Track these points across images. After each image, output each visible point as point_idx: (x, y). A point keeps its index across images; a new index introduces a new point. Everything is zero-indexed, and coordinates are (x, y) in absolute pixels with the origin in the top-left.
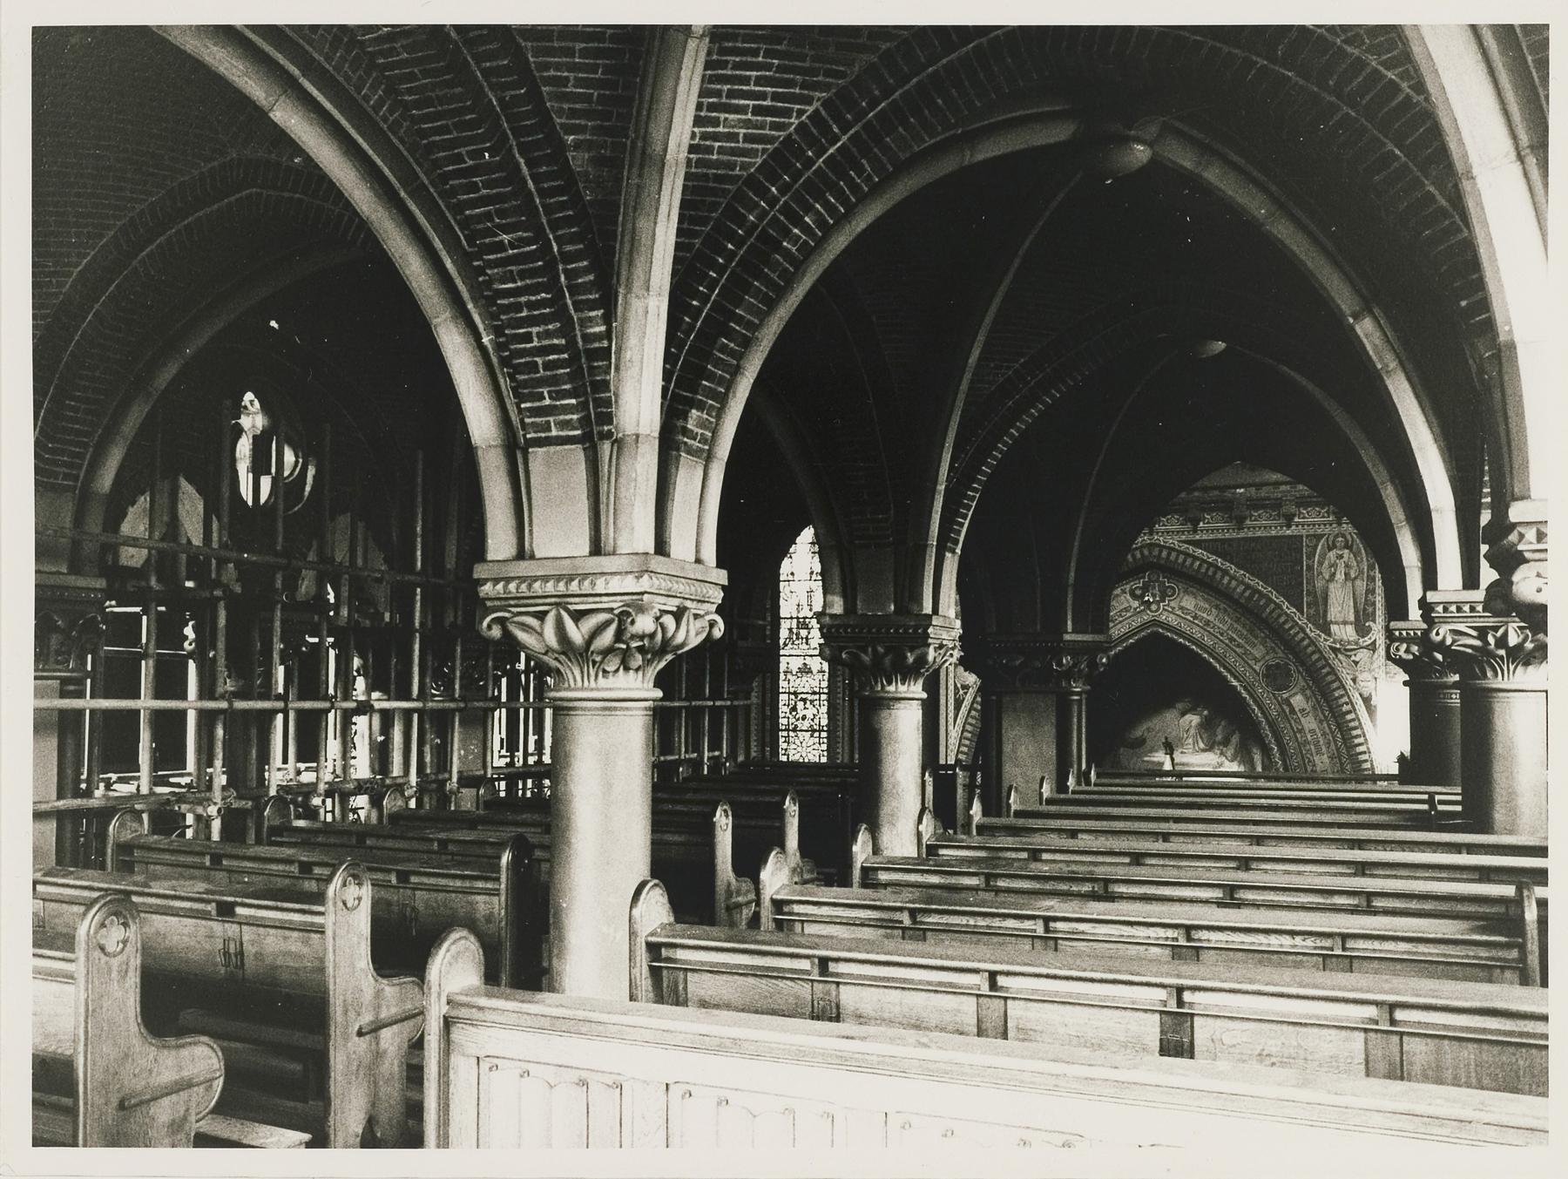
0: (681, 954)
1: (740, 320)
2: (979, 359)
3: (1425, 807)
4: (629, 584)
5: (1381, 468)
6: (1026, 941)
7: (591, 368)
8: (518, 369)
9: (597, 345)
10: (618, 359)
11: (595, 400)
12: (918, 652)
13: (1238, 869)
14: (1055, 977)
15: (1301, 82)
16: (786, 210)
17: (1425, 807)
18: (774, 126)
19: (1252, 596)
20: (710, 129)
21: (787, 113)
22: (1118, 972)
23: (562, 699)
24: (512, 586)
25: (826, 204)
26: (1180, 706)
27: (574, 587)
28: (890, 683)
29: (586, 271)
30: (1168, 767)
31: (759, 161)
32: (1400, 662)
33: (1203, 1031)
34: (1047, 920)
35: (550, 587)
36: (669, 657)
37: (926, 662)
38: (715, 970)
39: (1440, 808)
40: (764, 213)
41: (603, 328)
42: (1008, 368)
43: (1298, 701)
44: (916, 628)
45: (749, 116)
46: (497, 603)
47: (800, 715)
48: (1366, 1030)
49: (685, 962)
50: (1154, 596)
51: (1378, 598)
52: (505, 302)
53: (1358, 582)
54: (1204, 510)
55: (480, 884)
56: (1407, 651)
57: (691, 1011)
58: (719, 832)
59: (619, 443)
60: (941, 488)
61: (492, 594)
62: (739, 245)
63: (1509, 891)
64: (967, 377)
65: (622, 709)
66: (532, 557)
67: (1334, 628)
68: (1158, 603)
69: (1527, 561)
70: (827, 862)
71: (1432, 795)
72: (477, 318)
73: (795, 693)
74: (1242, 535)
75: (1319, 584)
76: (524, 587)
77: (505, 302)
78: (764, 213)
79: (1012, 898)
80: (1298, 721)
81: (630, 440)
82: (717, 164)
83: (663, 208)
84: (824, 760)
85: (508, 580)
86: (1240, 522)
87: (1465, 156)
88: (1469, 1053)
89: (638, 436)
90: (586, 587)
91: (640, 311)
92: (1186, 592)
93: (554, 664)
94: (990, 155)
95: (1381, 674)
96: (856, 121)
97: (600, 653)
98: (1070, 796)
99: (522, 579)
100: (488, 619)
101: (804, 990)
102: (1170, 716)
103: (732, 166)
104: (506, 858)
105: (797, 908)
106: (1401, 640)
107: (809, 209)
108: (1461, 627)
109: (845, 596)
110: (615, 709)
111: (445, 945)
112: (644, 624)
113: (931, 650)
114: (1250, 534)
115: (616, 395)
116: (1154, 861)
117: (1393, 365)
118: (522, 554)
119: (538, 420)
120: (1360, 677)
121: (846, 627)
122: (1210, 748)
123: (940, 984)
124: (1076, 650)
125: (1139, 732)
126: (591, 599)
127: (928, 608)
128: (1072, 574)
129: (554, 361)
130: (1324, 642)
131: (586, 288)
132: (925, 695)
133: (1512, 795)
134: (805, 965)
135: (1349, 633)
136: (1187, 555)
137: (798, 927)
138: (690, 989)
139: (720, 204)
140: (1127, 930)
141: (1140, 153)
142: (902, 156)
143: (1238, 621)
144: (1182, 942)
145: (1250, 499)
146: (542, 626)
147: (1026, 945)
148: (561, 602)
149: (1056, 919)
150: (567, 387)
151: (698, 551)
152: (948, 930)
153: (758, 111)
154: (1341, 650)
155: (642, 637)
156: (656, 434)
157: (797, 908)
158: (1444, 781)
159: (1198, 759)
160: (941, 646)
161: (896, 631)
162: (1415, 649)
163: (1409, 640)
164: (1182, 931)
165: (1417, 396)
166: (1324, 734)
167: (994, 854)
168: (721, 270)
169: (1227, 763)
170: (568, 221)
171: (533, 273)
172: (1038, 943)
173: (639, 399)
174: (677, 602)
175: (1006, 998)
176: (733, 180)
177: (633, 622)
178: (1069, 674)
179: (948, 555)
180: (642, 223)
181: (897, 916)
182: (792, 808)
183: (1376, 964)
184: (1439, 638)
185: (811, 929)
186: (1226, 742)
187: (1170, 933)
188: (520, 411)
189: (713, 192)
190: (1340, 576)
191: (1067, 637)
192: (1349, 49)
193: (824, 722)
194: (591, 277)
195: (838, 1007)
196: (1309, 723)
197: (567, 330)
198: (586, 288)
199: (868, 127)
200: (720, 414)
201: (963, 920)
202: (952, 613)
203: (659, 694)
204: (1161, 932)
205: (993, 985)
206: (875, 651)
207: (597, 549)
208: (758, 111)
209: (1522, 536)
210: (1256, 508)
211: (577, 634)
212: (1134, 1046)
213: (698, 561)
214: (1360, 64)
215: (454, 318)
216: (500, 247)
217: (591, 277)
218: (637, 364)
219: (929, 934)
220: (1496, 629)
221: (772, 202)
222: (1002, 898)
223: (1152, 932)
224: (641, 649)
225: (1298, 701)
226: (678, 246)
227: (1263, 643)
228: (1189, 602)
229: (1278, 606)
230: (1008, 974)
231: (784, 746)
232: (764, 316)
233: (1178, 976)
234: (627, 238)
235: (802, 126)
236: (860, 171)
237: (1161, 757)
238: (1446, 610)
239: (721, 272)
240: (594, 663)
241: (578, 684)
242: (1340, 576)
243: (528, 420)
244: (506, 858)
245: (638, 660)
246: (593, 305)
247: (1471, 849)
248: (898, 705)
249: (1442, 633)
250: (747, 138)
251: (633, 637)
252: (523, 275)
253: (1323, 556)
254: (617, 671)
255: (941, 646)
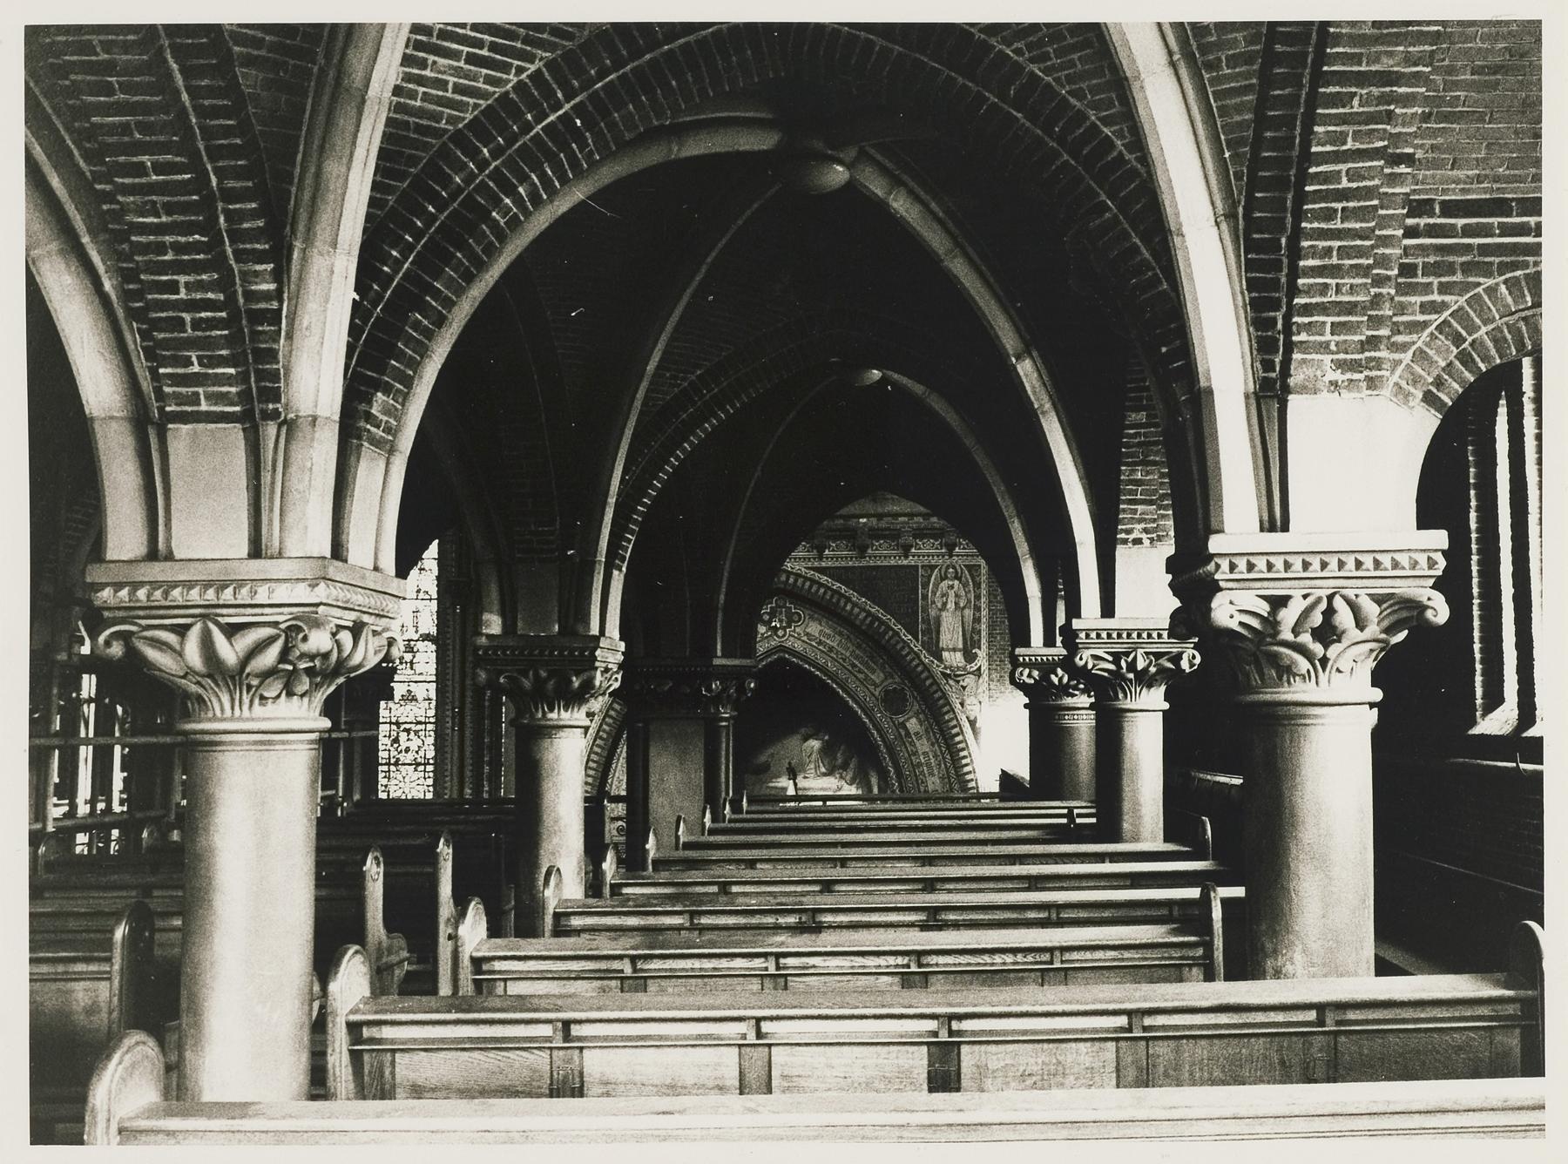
0: (387, 1032)
1: (437, 294)
2: (658, 368)
3: (1064, 821)
4: (302, 594)
5: (1009, 502)
6: (755, 980)
7: (255, 335)
8: (157, 325)
9: (263, 305)
10: (291, 324)
11: (257, 372)
12: (585, 676)
13: (821, 892)
14: (827, 1017)
15: (1028, 124)
16: (497, 175)
17: (1064, 821)
18: (489, 80)
19: (872, 623)
20: (416, 71)
21: (505, 68)
22: (891, 1006)
23: (195, 732)
24: (142, 594)
25: (543, 177)
26: (803, 730)
27: (227, 596)
28: (552, 710)
29: (254, 215)
30: (791, 792)
31: (469, 117)
32: (1022, 687)
33: (969, 1057)
34: (778, 956)
35: (194, 595)
36: (341, 680)
37: (593, 687)
38: (430, 1047)
39: (1078, 821)
40: (472, 176)
41: (272, 287)
42: (684, 379)
43: (913, 724)
44: (582, 651)
45: (462, 64)
46: (121, 614)
47: (403, 747)
48: (1117, 1040)
49: (393, 1041)
50: (781, 621)
51: (983, 627)
52: (142, 239)
53: (967, 612)
54: (829, 538)
55: (80, 967)
56: (1030, 676)
57: (401, 1103)
58: (369, 885)
59: (290, 427)
60: (612, 500)
61: (112, 602)
62: (440, 210)
63: (1194, 893)
64: (644, 385)
65: (283, 742)
66: (169, 557)
67: (945, 654)
68: (784, 629)
69: (1221, 589)
70: (516, 912)
71: (1071, 809)
72: (96, 259)
73: (398, 724)
74: (864, 563)
75: (933, 613)
76: (158, 594)
77: (142, 239)
78: (472, 176)
79: (739, 936)
80: (912, 744)
81: (304, 424)
82: (420, 113)
83: (360, 153)
84: (430, 796)
85: (135, 586)
86: (862, 551)
87: (1177, 215)
88: (1201, 1050)
89: (315, 419)
90: (244, 596)
91: (324, 274)
92: (811, 617)
93: (194, 688)
94: (696, 152)
95: (984, 698)
96: (583, 89)
97: (257, 676)
98: (726, 824)
99: (155, 585)
100: (108, 632)
101: (540, 1060)
102: (793, 742)
103: (437, 117)
104: (120, 933)
105: (498, 965)
106: (1025, 665)
107: (524, 178)
108: (1100, 653)
109: (503, 614)
110: (270, 743)
111: (116, 1057)
112: (319, 641)
113: (598, 673)
114: (872, 563)
115: (288, 371)
116: (843, 888)
117: (1048, 406)
118: (153, 555)
119: (183, 390)
120: (968, 701)
121: (504, 649)
122: (829, 773)
123: (699, 1037)
124: (725, 674)
125: (763, 758)
126: (249, 611)
127: (595, 630)
128: (722, 597)
129: (208, 320)
130: (937, 669)
131: (254, 235)
132: (1166, 706)
133: (1136, 804)
134: (546, 1030)
135: (956, 659)
136: (813, 581)
137: (500, 990)
138: (398, 1077)
139: (421, 159)
140: (859, 961)
141: (838, 174)
142: (628, 136)
143: (859, 647)
144: (914, 968)
145: (871, 529)
146: (182, 643)
147: (755, 985)
148: (208, 614)
149: (786, 955)
150: (224, 352)
151: (376, 558)
152: (672, 976)
153: (472, 59)
154: (953, 675)
155: (312, 657)
156: (337, 417)
157: (498, 965)
158: (1077, 797)
159: (818, 783)
160: (607, 670)
161: (561, 654)
162: (1036, 673)
163: (1031, 666)
164: (627, 962)
165: (1066, 436)
166: (935, 756)
167: (681, 890)
168: (418, 235)
169: (846, 786)
170: (233, 152)
171: (185, 208)
172: (768, 983)
173: (316, 373)
174: (353, 616)
175: (770, 1045)
176: (438, 133)
177: (305, 639)
178: (718, 700)
179: (616, 573)
180: (332, 168)
181: (616, 965)
182: (445, 850)
183: (1087, 974)
184: (1082, 663)
185: (515, 988)
186: (845, 767)
187: (900, 960)
188: (155, 376)
189: (415, 144)
190: (951, 606)
191: (717, 662)
192: (1073, 101)
193: (431, 754)
194: (261, 223)
195: (581, 1074)
196: (923, 746)
197: (225, 284)
198: (254, 235)
199: (594, 97)
200: (405, 398)
201: (697, 964)
202: (616, 635)
203: (326, 723)
204: (891, 960)
205: (567, 1037)
206: (537, 675)
207: (256, 552)
208: (472, 59)
209: (1218, 566)
210: (878, 538)
211: (229, 653)
212: (902, 1080)
213: (376, 569)
214: (1081, 117)
215: (61, 252)
216: (140, 170)
217: (261, 223)
218: (316, 330)
219: (650, 982)
220: (1127, 654)
221: (481, 165)
222: (707, 936)
223: (882, 961)
224: (310, 672)
225: (913, 724)
226: (372, 202)
227: (883, 669)
228: (814, 628)
229: (897, 634)
230: (771, 1019)
231: (384, 782)
232: (460, 291)
233: (950, 1005)
234: (309, 181)
235: (520, 87)
236: (583, 145)
237: (785, 783)
238: (1087, 636)
239: (418, 235)
240: (249, 687)
241: (224, 714)
242: (951, 606)
243: (167, 389)
244: (120, 933)
245: (304, 684)
246: (261, 258)
247: (1100, 858)
248: (561, 734)
249: (1084, 658)
250: (458, 89)
251: (303, 656)
252: (169, 209)
253: (936, 586)
254: (279, 696)
255: (607, 670)
